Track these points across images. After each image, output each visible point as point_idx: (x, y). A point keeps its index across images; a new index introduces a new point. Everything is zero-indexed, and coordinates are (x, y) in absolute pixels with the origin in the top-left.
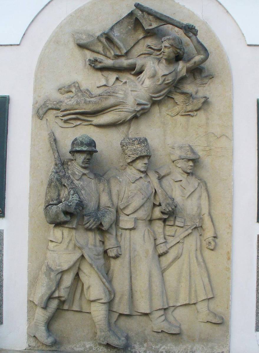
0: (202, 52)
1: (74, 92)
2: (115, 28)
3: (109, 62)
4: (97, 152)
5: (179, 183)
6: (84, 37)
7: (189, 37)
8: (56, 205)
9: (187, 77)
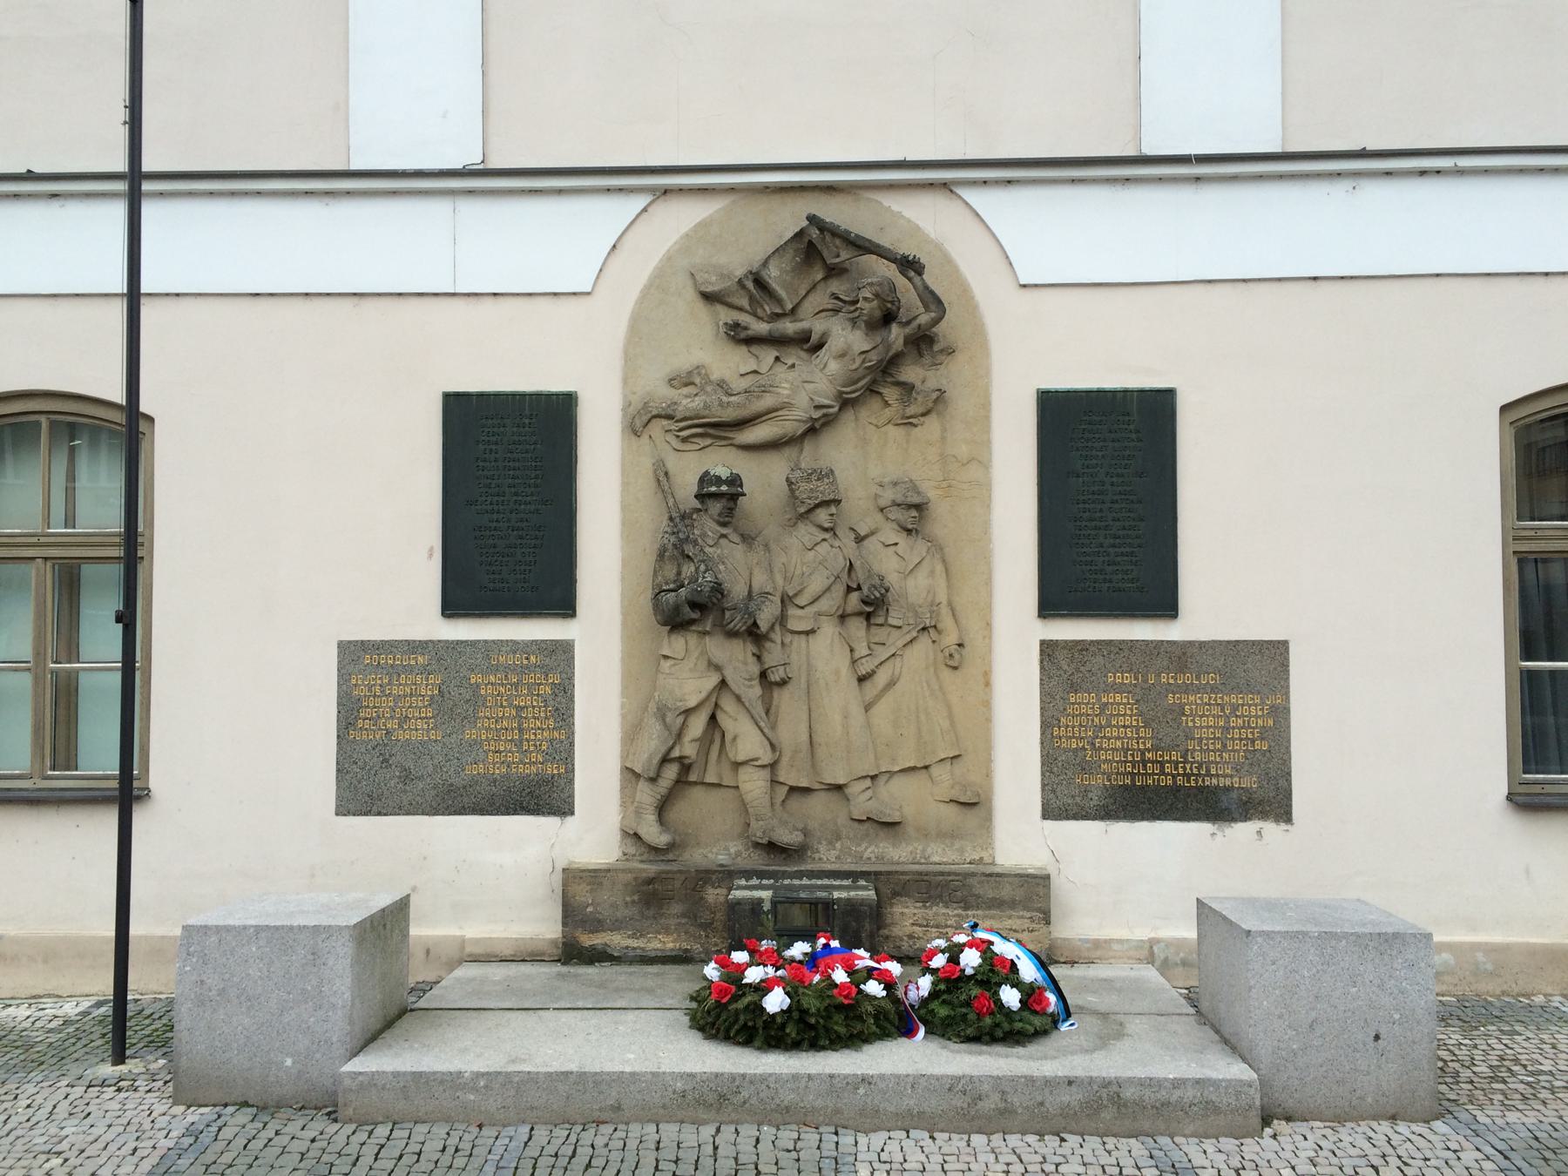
0: (933, 307)
1: (699, 385)
2: (771, 261)
3: (761, 328)
4: (745, 495)
5: (893, 548)
6: (714, 278)
7: (910, 279)
8: (672, 591)
9: (904, 353)
